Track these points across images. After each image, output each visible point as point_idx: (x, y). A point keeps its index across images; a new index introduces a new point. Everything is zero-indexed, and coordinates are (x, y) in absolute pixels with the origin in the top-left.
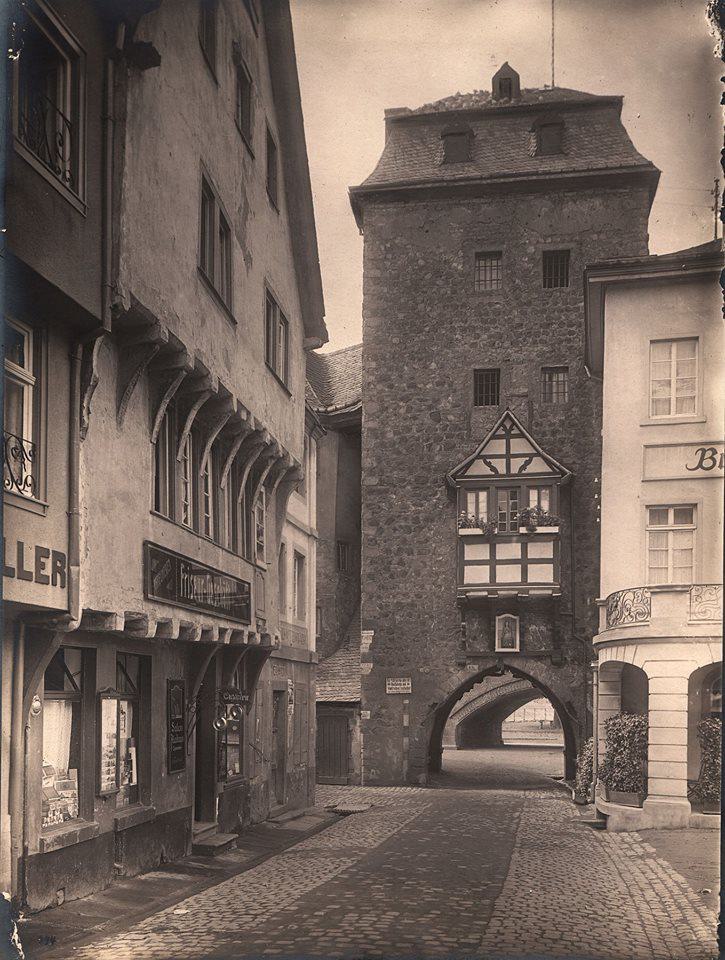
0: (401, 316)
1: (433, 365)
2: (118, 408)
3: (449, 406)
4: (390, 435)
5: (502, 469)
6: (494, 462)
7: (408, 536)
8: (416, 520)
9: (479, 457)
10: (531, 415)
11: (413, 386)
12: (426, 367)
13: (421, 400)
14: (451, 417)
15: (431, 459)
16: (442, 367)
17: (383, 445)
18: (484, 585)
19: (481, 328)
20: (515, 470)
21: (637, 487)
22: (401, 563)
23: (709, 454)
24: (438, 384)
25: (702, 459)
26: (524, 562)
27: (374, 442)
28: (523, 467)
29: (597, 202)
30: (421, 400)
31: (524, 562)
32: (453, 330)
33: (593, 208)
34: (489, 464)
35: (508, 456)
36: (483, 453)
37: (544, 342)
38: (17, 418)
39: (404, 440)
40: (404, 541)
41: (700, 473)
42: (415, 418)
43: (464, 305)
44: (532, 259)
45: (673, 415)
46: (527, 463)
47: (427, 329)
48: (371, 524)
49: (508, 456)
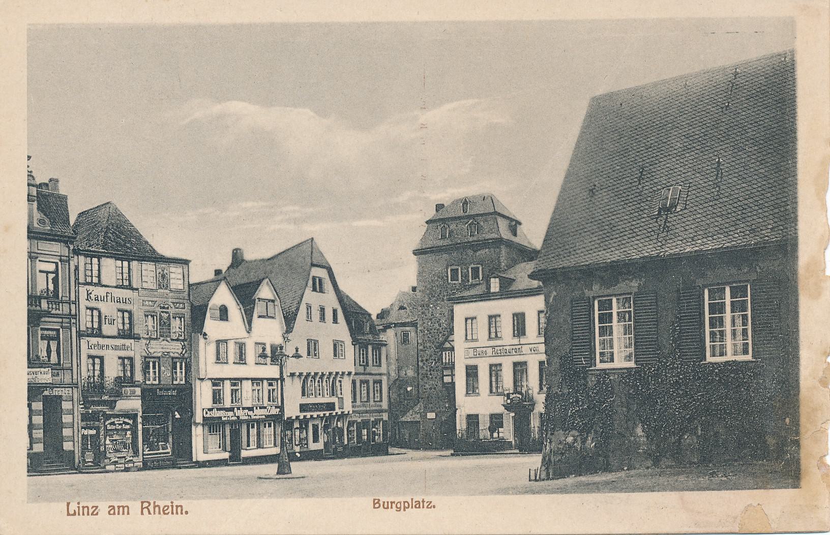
4: (426, 332)
22: (431, 374)
24: (440, 314)
34: (450, 343)
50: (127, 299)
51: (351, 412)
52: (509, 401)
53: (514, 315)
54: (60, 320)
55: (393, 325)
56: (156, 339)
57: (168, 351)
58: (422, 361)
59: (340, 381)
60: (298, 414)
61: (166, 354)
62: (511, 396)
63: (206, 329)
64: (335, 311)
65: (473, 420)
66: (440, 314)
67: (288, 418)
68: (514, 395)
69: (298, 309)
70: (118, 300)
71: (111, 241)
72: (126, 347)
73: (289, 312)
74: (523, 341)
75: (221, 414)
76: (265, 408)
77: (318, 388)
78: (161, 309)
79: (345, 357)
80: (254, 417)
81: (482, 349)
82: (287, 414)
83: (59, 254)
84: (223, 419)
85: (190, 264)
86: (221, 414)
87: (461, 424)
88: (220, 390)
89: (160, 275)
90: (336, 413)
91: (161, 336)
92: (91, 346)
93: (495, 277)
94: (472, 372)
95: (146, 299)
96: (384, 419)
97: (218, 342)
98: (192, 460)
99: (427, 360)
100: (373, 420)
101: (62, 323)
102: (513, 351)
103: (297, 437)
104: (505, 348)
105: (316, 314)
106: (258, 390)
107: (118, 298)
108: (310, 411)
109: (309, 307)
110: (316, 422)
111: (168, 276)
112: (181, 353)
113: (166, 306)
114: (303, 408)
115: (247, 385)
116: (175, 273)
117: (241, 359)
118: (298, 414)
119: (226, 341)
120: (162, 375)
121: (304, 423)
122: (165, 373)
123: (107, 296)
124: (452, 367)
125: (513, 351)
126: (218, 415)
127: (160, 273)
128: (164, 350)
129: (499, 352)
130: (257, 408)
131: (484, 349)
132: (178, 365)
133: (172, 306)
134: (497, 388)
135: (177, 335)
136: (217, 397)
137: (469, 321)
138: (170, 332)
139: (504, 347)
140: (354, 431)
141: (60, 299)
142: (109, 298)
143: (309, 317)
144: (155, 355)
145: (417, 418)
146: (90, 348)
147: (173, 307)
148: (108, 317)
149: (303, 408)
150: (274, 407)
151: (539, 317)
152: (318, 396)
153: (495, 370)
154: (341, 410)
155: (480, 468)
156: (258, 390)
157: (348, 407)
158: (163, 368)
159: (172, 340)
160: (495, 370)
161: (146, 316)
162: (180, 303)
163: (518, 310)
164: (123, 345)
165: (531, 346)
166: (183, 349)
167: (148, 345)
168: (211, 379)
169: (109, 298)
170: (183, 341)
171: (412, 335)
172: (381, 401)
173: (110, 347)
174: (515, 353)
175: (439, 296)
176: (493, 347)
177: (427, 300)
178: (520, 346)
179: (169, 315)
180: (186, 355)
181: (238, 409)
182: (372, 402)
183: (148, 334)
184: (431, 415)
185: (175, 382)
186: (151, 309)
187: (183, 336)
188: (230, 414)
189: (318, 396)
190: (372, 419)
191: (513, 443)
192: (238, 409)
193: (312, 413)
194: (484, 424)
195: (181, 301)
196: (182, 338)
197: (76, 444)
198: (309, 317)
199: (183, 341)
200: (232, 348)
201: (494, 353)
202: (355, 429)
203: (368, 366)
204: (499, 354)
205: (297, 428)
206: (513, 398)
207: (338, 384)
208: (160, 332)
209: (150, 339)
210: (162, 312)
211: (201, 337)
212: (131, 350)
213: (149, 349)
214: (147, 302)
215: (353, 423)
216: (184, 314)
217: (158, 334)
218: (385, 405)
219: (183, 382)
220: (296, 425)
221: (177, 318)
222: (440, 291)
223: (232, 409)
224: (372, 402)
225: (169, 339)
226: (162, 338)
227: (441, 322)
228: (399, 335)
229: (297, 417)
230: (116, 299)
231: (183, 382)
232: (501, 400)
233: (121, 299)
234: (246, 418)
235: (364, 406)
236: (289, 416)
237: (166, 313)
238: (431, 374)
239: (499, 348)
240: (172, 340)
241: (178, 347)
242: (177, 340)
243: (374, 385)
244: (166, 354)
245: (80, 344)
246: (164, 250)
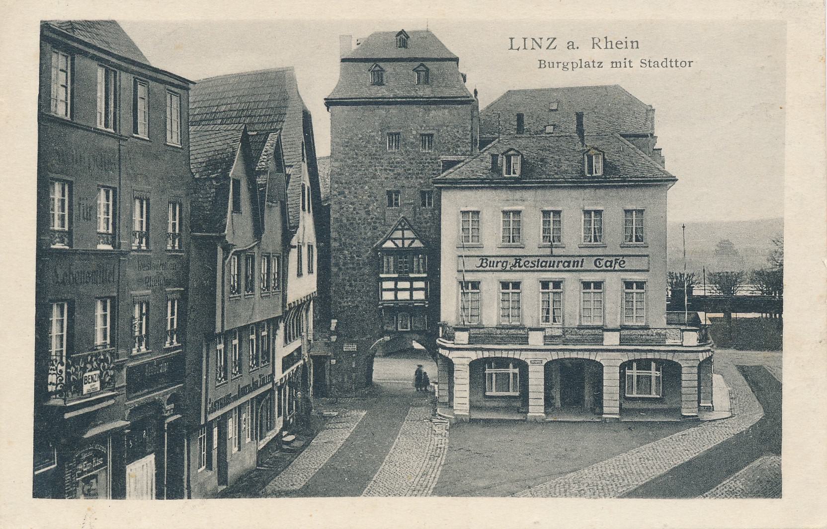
6: (397, 242)
8: (358, 264)
9: (389, 239)
10: (415, 214)
15: (366, 234)
16: (370, 188)
17: (341, 226)
18: (392, 300)
19: (390, 170)
20: (406, 245)
23: (485, 261)
25: (482, 263)
26: (411, 290)
28: (411, 244)
31: (411, 290)
34: (394, 243)
35: (403, 239)
36: (392, 237)
37: (421, 178)
41: (481, 268)
44: (415, 137)
45: (470, 243)
46: (413, 242)
49: (403, 239)
107: (571, 44)
175: (367, 170)
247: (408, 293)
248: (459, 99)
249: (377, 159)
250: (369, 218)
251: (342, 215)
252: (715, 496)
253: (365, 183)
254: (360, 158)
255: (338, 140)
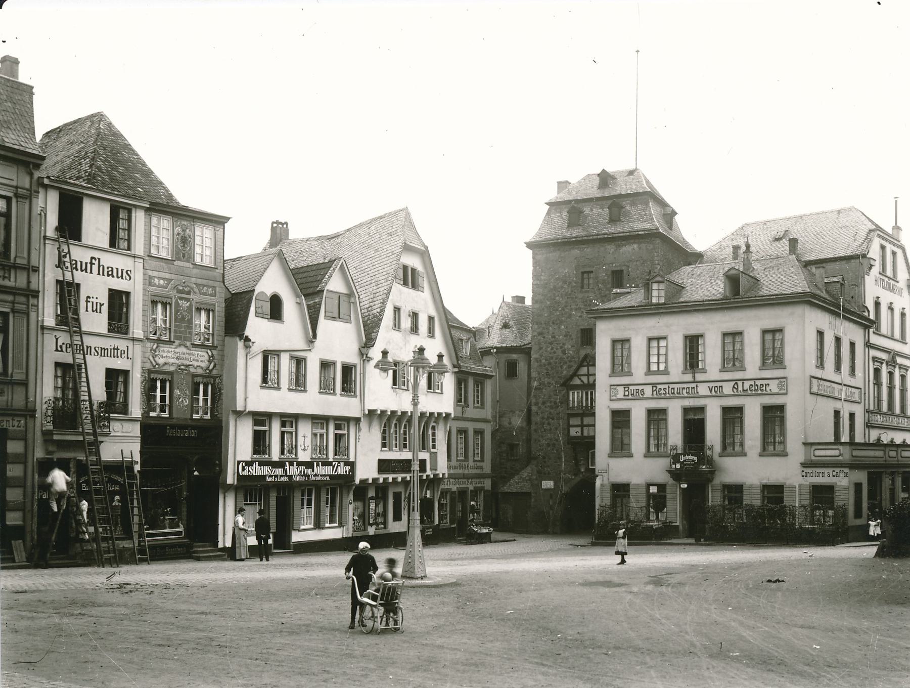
0: (549, 303)
1: (563, 327)
2: (369, 428)
3: (570, 346)
4: (544, 361)
5: (585, 380)
7: (552, 411)
8: (555, 403)
11: (553, 337)
12: (559, 328)
13: (557, 344)
14: (571, 352)
16: (567, 328)
17: (540, 366)
21: (608, 403)
22: (549, 424)
24: (565, 336)
27: (536, 364)
29: (635, 246)
30: (557, 344)
32: (571, 310)
33: (633, 249)
34: (580, 379)
38: (210, 271)
39: (550, 364)
40: (550, 413)
42: (555, 352)
43: (576, 298)
47: (560, 309)
48: (535, 405)
50: (124, 272)
51: (446, 476)
52: (678, 466)
53: (686, 337)
54: (10, 298)
55: (495, 350)
56: (170, 342)
57: (188, 363)
58: (536, 404)
59: (433, 428)
60: (376, 475)
61: (183, 367)
62: (682, 459)
63: (248, 332)
64: (431, 319)
65: (620, 490)
66: (565, 336)
67: (361, 481)
68: (687, 457)
69: (382, 310)
70: (110, 273)
71: (102, 172)
72: (119, 351)
73: (369, 315)
74: (699, 377)
75: (265, 471)
76: (330, 464)
77: (394, 435)
78: (177, 293)
79: (442, 390)
80: (314, 478)
81: (637, 387)
82: (359, 476)
83: (14, 183)
84: (268, 479)
85: (226, 224)
86: (265, 471)
87: (602, 498)
88: (264, 432)
89: (179, 237)
90: (427, 476)
91: (177, 338)
92: (61, 347)
93: (659, 282)
94: (620, 419)
95: (155, 274)
96: (486, 489)
97: (267, 355)
98: (217, 546)
99: (544, 403)
100: (473, 489)
101: (13, 302)
102: (685, 391)
103: (372, 512)
104: (672, 386)
105: (406, 323)
106: (322, 435)
107: (110, 269)
108: (393, 472)
109: (397, 310)
110: (398, 490)
111: (192, 241)
112: (208, 368)
113: (187, 289)
114: (384, 466)
115: (305, 430)
116: (203, 236)
117: (299, 384)
118: (375, 475)
119: (277, 353)
120: (176, 403)
121: (382, 489)
122: (180, 400)
123: (92, 264)
124: (589, 412)
125: (685, 391)
126: (260, 473)
127: (178, 234)
128: (179, 362)
129: (662, 392)
130: (318, 465)
131: (640, 388)
132: (201, 387)
133: (196, 290)
134: (657, 446)
135: (202, 338)
136: (260, 442)
137: (619, 346)
138: (191, 333)
139: (670, 385)
140: (446, 504)
141: (12, 261)
142: (95, 267)
143: (397, 325)
144: (166, 368)
145: (526, 488)
146: (59, 349)
147: (198, 291)
148: (91, 300)
149: (384, 466)
150: (342, 464)
151: (724, 343)
152: (394, 449)
153: (656, 417)
154: (434, 472)
155: (707, 574)
156: (322, 435)
157: (443, 468)
158: (177, 392)
159: (194, 345)
160: (656, 417)
161: (154, 303)
162: (209, 287)
163: (693, 331)
164: (114, 349)
165: (711, 385)
166: (210, 361)
167: (155, 351)
168: (254, 414)
169: (95, 267)
170: (213, 347)
171: (522, 367)
172: (482, 460)
173: (93, 350)
174: (686, 395)
175: (564, 310)
176: (654, 385)
177: (546, 315)
178: (694, 385)
179: (191, 305)
180: (215, 372)
181: (291, 464)
182: (471, 463)
183: (155, 334)
184: (548, 484)
185: (195, 416)
186: (165, 292)
187: (211, 340)
188: (279, 471)
189: (394, 449)
190: (471, 487)
191: (681, 528)
192: (291, 464)
193: (395, 476)
194: (636, 502)
195: (211, 283)
196: (210, 343)
197: (29, 516)
198: (397, 325)
199: (213, 347)
200: (286, 365)
201: (655, 393)
202: (448, 501)
203: (468, 406)
204: (663, 396)
205: (372, 498)
206: (685, 461)
207: (430, 432)
208: (175, 332)
209: (159, 341)
210: (181, 299)
211: (241, 344)
212: (128, 358)
213: (156, 359)
214: (156, 279)
215: (446, 493)
216: (214, 305)
217: (173, 334)
218: (487, 467)
219: (208, 417)
220: (371, 493)
221: (203, 312)
222: (566, 302)
223: (280, 464)
224: (471, 463)
225: (188, 344)
226: (177, 342)
227: (566, 347)
228: (502, 365)
229: (375, 480)
230: (106, 270)
231: (208, 417)
232: (664, 463)
233: (115, 271)
234: (301, 479)
235: (461, 467)
236: (365, 477)
237: (187, 300)
238: (549, 424)
239: (662, 387)
240: (194, 345)
241: (203, 359)
242: (202, 346)
243: (457, 435)
244: (183, 369)
245: (44, 281)
246: (184, 198)
247: (585, 423)
248: (591, 237)
249: (572, 298)
250: (565, 357)
251: (541, 356)
252: (170, 196)
253: (561, 322)
254: (557, 298)
255: (538, 282)
